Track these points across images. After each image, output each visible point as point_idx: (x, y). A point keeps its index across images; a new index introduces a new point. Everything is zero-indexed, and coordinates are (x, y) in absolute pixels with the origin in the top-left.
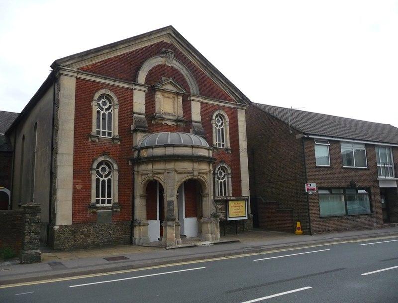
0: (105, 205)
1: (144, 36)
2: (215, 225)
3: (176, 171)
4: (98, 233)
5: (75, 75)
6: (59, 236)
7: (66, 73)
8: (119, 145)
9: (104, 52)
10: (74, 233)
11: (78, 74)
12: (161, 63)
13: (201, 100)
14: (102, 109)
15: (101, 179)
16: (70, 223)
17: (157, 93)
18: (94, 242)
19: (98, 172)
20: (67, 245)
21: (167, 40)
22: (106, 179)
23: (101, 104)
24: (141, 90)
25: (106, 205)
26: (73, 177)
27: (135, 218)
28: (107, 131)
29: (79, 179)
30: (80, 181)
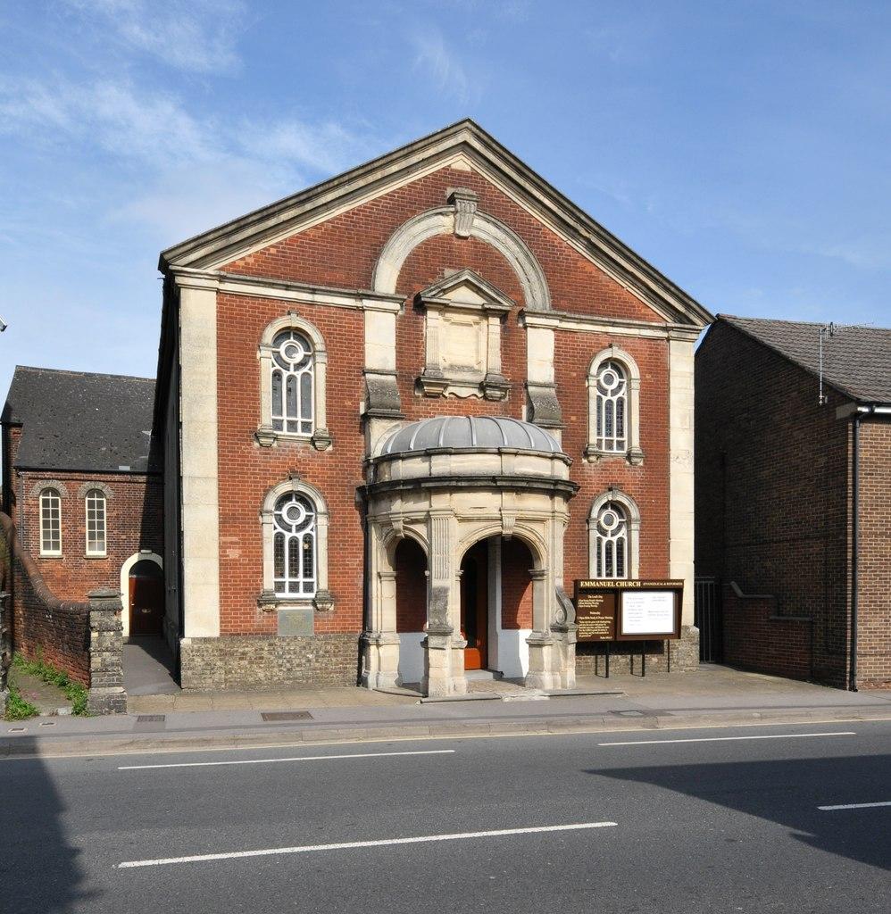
4: (281, 657)
5: (216, 284)
6: (193, 660)
12: (441, 231)
13: (555, 323)
14: (604, 533)
16: (216, 633)
20: (210, 681)
24: (385, 311)
25: (301, 594)
29: (235, 535)
30: (235, 539)
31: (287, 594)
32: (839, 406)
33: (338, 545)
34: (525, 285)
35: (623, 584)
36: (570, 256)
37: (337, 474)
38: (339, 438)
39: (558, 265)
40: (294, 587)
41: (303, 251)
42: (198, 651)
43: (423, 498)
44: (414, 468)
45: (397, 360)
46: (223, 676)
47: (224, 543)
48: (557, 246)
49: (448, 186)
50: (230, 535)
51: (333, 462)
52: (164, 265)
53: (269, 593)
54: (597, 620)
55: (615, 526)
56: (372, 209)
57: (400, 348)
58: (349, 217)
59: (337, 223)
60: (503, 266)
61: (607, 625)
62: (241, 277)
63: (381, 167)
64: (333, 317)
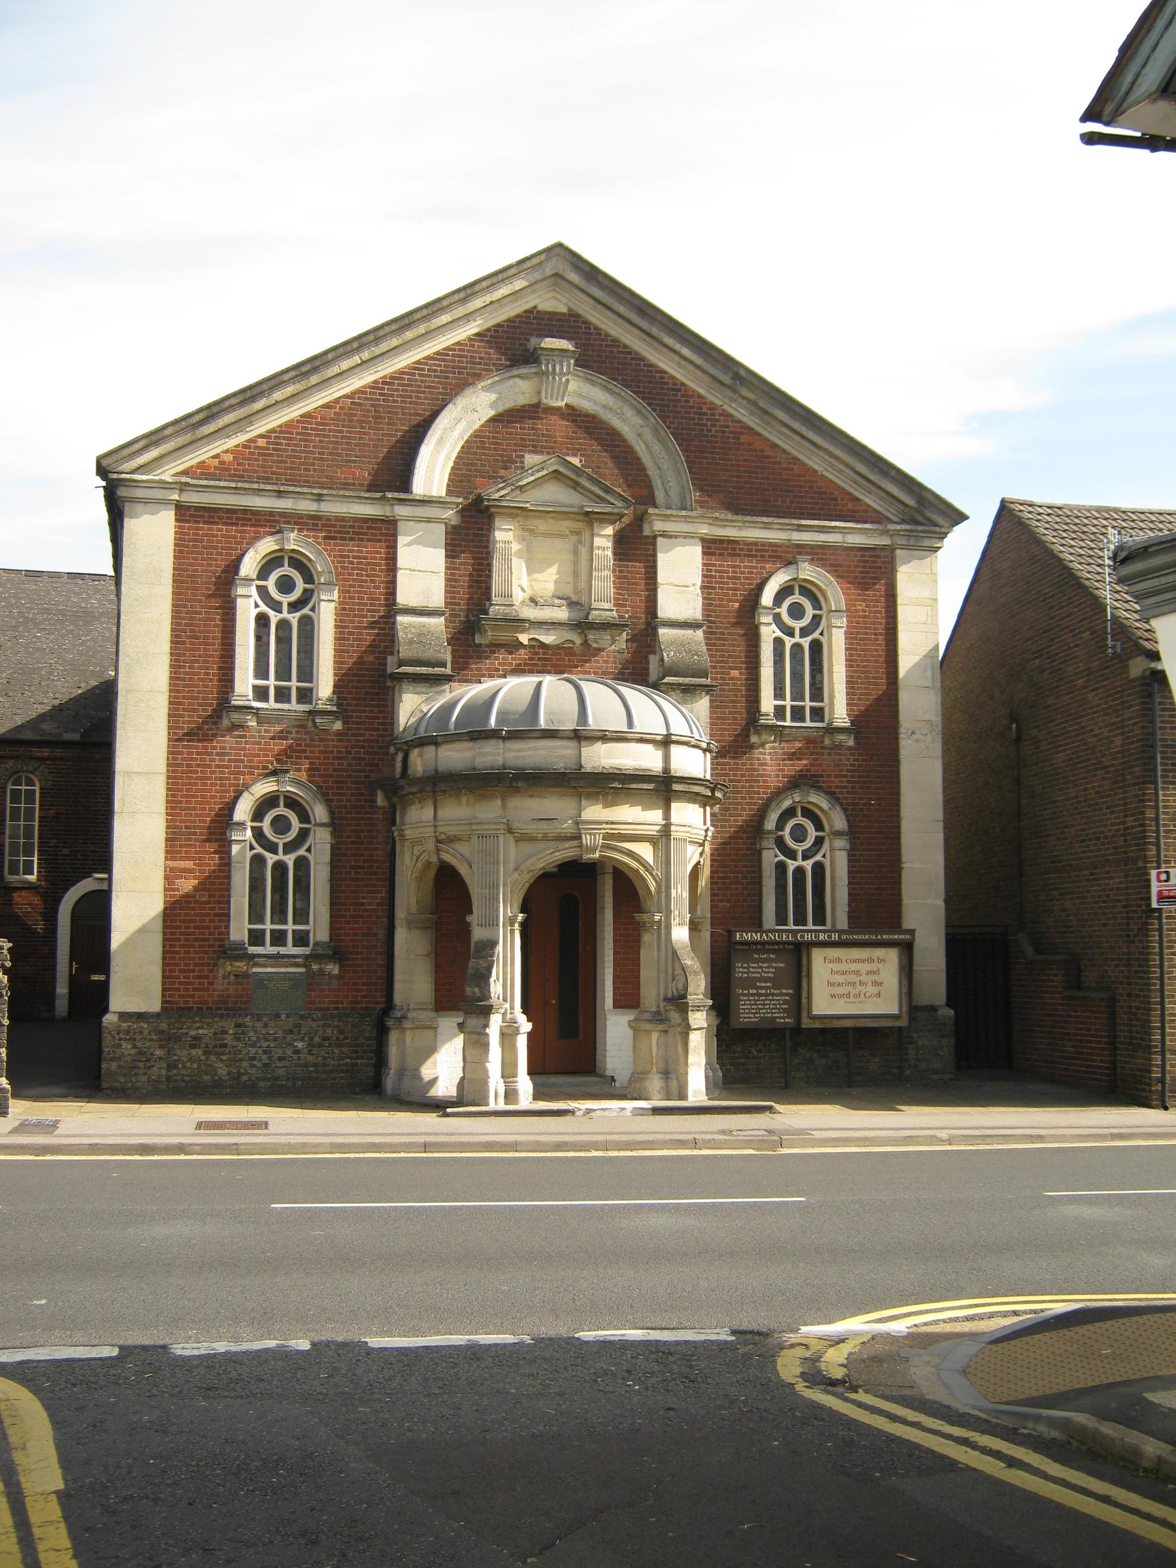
0: (282, 950)
1: (651, 313)
2: (678, 1038)
3: (510, 831)
4: (253, 1045)
6: (119, 1046)
7: (139, 493)
8: (338, 733)
9: (278, 396)
10: (168, 1039)
11: (181, 490)
14: (792, 855)
15: (792, 865)
16: (155, 1006)
17: (498, 522)
18: (239, 1074)
19: (780, 843)
20: (144, 1078)
21: (550, 302)
22: (808, 865)
23: (786, 618)
24: (429, 520)
25: (290, 949)
26: (167, 852)
27: (398, 998)
28: (808, 704)
29: (188, 859)
30: (189, 864)
31: (269, 949)
32: (1131, 658)
33: (348, 873)
34: (652, 472)
35: (808, 937)
36: (728, 427)
37: (349, 765)
38: (352, 711)
39: (708, 442)
40: (279, 938)
41: (306, 440)
42: (127, 1032)
43: (464, 799)
44: (454, 757)
45: (446, 592)
46: (164, 1072)
47: (172, 869)
48: (706, 414)
49: (532, 335)
50: (182, 859)
51: (343, 747)
52: (102, 471)
53: (240, 946)
54: (767, 995)
55: (809, 843)
56: (414, 374)
57: (341, 633)
58: (378, 388)
59: (359, 398)
60: (618, 446)
61: (785, 1002)
62: (212, 483)
63: (425, 318)
64: (348, 532)
